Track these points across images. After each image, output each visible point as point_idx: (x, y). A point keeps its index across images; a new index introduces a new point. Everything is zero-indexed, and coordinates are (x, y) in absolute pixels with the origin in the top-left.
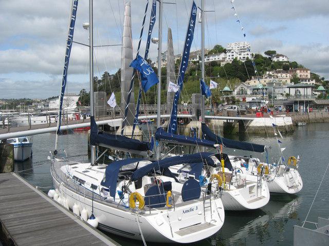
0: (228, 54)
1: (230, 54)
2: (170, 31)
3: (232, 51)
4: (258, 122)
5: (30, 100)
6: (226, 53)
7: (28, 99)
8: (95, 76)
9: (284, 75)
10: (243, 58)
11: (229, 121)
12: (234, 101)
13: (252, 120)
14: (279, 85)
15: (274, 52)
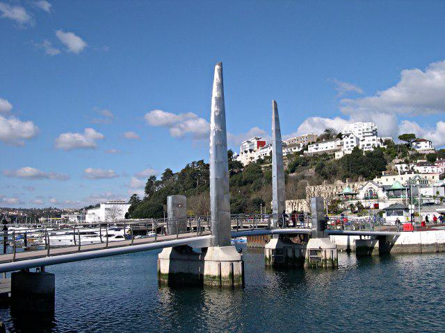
0: (345, 140)
1: (348, 140)
2: (275, 103)
3: (351, 136)
4: (406, 238)
5: (58, 209)
6: (342, 139)
7: (55, 209)
8: (101, 205)
9: (429, 169)
10: (368, 145)
11: (363, 238)
12: (361, 210)
13: (398, 236)
14: (424, 183)
15: (412, 136)
